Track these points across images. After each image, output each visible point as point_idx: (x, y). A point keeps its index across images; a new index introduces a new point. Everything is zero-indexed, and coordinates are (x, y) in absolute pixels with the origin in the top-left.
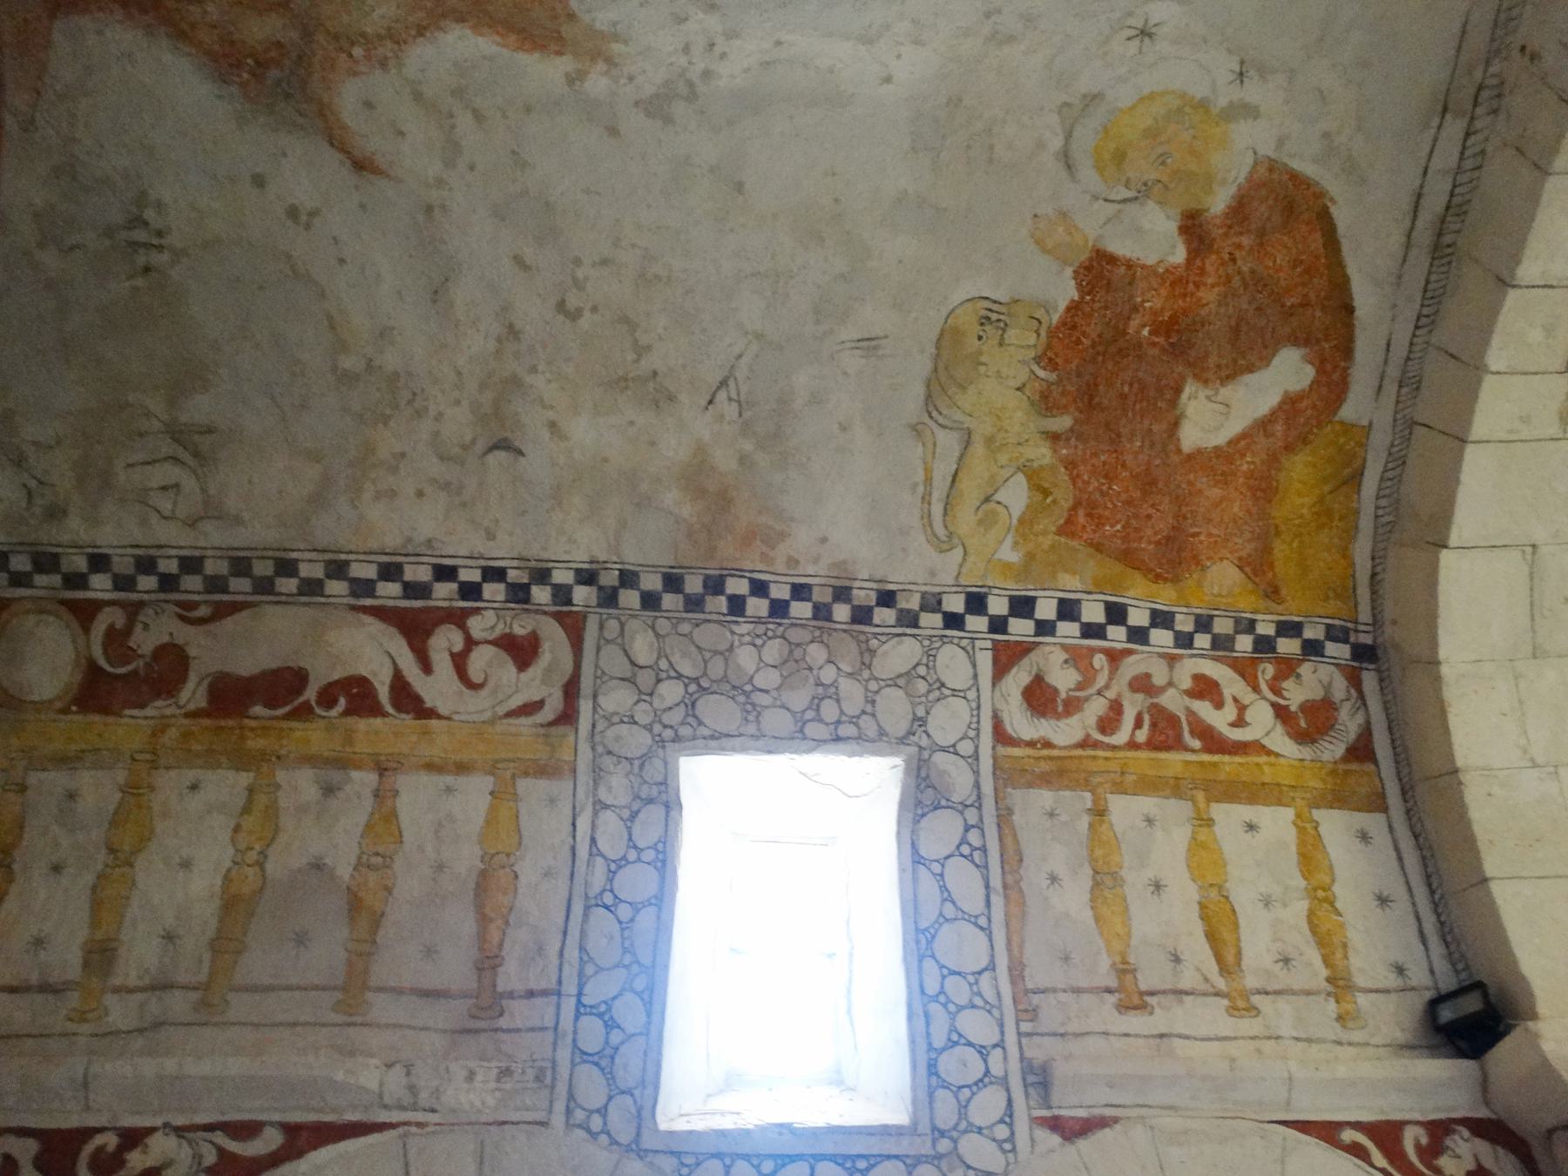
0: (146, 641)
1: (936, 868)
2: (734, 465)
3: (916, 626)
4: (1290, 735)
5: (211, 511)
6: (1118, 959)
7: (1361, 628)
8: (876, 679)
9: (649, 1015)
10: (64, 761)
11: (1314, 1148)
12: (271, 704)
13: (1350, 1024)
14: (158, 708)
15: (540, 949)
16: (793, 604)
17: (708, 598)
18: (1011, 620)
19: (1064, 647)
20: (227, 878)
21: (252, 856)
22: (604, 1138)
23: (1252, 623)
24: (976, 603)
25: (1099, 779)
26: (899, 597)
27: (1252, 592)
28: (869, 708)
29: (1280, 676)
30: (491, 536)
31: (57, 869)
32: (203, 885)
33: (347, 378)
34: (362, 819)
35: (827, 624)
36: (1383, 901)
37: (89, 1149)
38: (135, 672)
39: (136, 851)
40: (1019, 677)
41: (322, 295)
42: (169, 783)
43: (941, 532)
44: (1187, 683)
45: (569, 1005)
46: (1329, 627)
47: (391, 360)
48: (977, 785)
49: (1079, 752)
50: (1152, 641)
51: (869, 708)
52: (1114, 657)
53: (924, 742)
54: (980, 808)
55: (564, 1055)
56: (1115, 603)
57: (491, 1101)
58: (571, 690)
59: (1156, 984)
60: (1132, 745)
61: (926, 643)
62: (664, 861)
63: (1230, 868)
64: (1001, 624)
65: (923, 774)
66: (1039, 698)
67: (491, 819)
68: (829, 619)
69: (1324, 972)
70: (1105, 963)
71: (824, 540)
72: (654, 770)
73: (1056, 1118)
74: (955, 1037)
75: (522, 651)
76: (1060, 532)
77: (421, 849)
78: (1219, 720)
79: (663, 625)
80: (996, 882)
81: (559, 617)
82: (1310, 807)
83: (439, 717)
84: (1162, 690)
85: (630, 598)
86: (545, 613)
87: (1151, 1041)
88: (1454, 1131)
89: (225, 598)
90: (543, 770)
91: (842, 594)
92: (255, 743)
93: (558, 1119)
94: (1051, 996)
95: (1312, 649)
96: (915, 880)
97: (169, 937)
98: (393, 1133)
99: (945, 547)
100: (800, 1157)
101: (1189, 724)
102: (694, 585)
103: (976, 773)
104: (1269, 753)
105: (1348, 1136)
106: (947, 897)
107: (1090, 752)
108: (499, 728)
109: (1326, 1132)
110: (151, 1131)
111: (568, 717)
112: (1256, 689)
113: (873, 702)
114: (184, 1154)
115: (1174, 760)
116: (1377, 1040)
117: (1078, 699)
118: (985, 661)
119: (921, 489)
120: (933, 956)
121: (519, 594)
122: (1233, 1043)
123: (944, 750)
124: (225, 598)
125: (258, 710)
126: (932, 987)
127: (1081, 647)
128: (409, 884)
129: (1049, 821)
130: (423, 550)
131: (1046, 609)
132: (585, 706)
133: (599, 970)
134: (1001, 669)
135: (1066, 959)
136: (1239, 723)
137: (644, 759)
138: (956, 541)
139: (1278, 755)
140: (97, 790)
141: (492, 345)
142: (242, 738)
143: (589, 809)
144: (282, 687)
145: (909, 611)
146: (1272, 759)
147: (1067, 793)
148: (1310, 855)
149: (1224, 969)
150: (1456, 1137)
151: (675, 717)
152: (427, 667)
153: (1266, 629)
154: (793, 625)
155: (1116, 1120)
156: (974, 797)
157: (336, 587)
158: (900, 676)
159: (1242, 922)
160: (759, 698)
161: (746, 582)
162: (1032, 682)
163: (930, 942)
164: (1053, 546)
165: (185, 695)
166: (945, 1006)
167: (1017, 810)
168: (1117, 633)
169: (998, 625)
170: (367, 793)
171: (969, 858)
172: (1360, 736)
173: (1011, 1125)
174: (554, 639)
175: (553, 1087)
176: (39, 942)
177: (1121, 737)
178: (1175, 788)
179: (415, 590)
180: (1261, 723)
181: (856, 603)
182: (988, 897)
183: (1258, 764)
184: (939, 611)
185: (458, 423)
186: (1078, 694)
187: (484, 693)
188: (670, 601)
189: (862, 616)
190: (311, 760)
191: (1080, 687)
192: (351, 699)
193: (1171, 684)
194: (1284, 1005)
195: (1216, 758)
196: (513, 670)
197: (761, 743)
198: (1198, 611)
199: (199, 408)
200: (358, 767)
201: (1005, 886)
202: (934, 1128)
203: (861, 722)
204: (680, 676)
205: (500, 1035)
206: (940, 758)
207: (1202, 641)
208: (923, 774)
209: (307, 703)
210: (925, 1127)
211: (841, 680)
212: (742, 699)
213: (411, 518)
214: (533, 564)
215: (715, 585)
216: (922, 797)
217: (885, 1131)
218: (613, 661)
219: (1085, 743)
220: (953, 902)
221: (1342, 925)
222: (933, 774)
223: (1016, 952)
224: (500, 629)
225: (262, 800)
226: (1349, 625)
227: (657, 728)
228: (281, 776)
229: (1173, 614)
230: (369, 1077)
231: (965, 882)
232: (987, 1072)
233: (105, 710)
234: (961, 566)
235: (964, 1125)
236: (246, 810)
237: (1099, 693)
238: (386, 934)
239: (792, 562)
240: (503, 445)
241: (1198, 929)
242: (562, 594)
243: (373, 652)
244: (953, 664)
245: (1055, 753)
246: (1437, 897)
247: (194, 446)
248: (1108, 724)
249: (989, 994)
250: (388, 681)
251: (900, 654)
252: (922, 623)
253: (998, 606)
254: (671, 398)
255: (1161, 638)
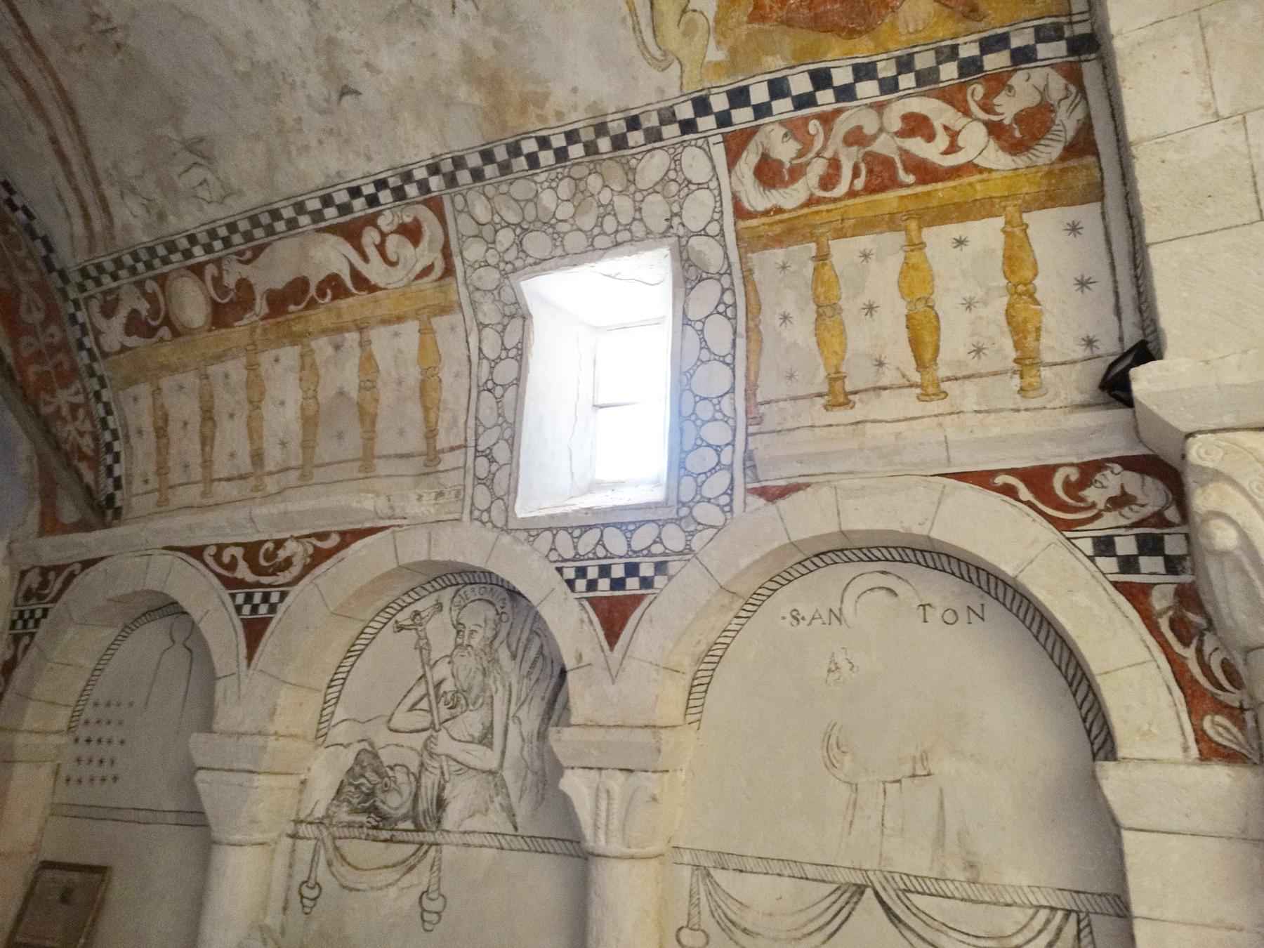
0: (230, 281)
1: (699, 326)
2: (493, 52)
3: (661, 139)
4: (1003, 148)
5: (229, 193)
6: (833, 370)
7: (1076, 18)
8: (641, 191)
9: (512, 451)
10: (219, 358)
11: (970, 492)
12: (297, 303)
13: (1031, 394)
14: (248, 318)
15: (455, 421)
16: (570, 148)
17: (513, 161)
18: (734, 112)
19: (782, 123)
20: (302, 408)
21: (310, 393)
22: (489, 525)
23: (955, 48)
24: (702, 105)
25: (823, 230)
26: (642, 118)
27: (950, 17)
28: (638, 216)
29: (990, 94)
30: (369, 159)
31: (232, 416)
32: (291, 413)
33: (246, 78)
34: (356, 361)
35: (596, 157)
36: (1083, 284)
37: (262, 551)
38: (231, 300)
39: (260, 401)
40: (750, 159)
41: (205, 25)
42: (265, 359)
43: (657, 54)
44: (897, 125)
45: (471, 452)
46: (1037, 29)
47: (262, 55)
48: (726, 256)
49: (806, 211)
50: (859, 95)
51: (638, 216)
52: (827, 120)
53: (681, 231)
54: (730, 274)
55: (470, 480)
56: (818, 70)
57: (433, 511)
58: (446, 254)
59: (861, 385)
60: (852, 194)
61: (671, 151)
62: (521, 355)
63: (937, 281)
64: (723, 116)
65: (685, 256)
66: (769, 174)
67: (422, 347)
68: (597, 152)
69: (1013, 355)
70: (822, 374)
71: (575, 90)
72: (507, 295)
73: (763, 488)
74: (699, 442)
75: (412, 233)
76: (752, 19)
77: (389, 374)
78: (932, 152)
79: (490, 190)
80: (741, 328)
81: (426, 203)
82: (1022, 212)
83: (381, 289)
84: (874, 137)
85: (464, 176)
86: (418, 203)
87: (850, 428)
88: (1106, 468)
89: (256, 243)
90: (444, 310)
91: (601, 129)
92: (297, 328)
93: (466, 517)
94: (774, 405)
95: (1023, 56)
96: (683, 338)
97: (283, 444)
98: (387, 532)
99: (663, 65)
100: (595, 526)
101: (903, 162)
102: (501, 154)
103: (725, 247)
104: (981, 170)
105: (1000, 480)
106: (704, 345)
107: (815, 209)
108: (414, 288)
109: (982, 479)
110: (285, 540)
111: (449, 271)
112: (967, 113)
113: (640, 210)
114: (300, 549)
115: (890, 198)
116: (1057, 403)
117: (801, 165)
118: (719, 152)
119: (629, 21)
120: (690, 390)
121: (399, 194)
122: (920, 421)
123: (697, 234)
124: (256, 243)
125: (292, 308)
126: (687, 410)
127: (798, 118)
128: (387, 395)
129: (783, 274)
130: (336, 180)
131: (759, 94)
132: (457, 261)
133: (486, 429)
134: (733, 158)
135: (791, 376)
136: (953, 149)
137: (499, 288)
138: (670, 57)
139: (990, 171)
140: (235, 369)
141: (307, 20)
142: (290, 326)
143: (475, 329)
144: (297, 289)
145: (652, 128)
146: (985, 176)
147: (796, 247)
148: (1016, 257)
149: (921, 365)
150: (1108, 472)
151: (510, 256)
152: (366, 259)
153: (969, 50)
154: (574, 165)
155: (808, 485)
156: (726, 266)
157: (304, 220)
158: (657, 183)
159: (943, 325)
160: (563, 227)
161: (533, 140)
162: (760, 161)
163: (689, 380)
164: (749, 35)
165: (257, 308)
166: (694, 422)
167: (756, 270)
168: (826, 97)
169: (724, 120)
170: (356, 344)
171: (724, 314)
172: (1078, 132)
173: (731, 495)
174: (427, 217)
175: (463, 500)
176: (232, 455)
177: (842, 189)
178: (891, 222)
179: (344, 209)
180: (974, 142)
181: (612, 134)
182: (734, 341)
183: (970, 184)
184: (675, 122)
185: (316, 86)
186: (799, 161)
187: (400, 267)
188: (490, 170)
189: (619, 143)
190: (324, 332)
191: (801, 154)
192: (333, 289)
193: (881, 130)
194: (970, 387)
195: (929, 187)
196: (410, 246)
197: (567, 260)
198: (898, 53)
199: (191, 128)
200: (348, 331)
201: (747, 331)
202: (679, 502)
203: (633, 228)
204: (509, 225)
205: (441, 475)
206: (694, 241)
207: (907, 81)
208: (685, 256)
209: (312, 299)
210: (673, 502)
211: (615, 199)
212: (551, 230)
213: (322, 165)
214: (400, 170)
215: (514, 150)
216: (689, 275)
217: (647, 506)
218: (466, 226)
219: (811, 201)
220: (708, 349)
221: (1039, 314)
222: (692, 257)
223: (752, 378)
224: (396, 222)
225: (308, 360)
226: (1063, 20)
227: (502, 265)
228: (313, 344)
229: (874, 63)
230: (368, 503)
231: (719, 333)
232: (719, 463)
233: (227, 326)
234: (681, 77)
235: (698, 497)
236: (303, 368)
237: (818, 155)
238: (380, 426)
239: (560, 115)
240: (345, 91)
241: (903, 336)
242: (423, 186)
243: (332, 256)
244: (695, 164)
245: (786, 216)
246: (1139, 271)
247: (200, 151)
248: (828, 182)
249: (727, 409)
250: (348, 273)
251: (654, 165)
252: (665, 136)
253: (719, 103)
254: (428, 14)
255: (867, 89)
